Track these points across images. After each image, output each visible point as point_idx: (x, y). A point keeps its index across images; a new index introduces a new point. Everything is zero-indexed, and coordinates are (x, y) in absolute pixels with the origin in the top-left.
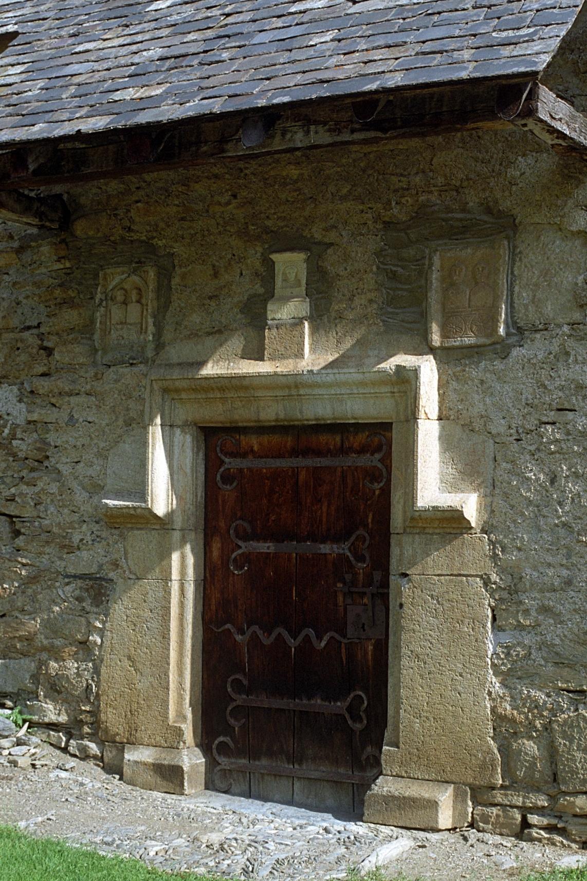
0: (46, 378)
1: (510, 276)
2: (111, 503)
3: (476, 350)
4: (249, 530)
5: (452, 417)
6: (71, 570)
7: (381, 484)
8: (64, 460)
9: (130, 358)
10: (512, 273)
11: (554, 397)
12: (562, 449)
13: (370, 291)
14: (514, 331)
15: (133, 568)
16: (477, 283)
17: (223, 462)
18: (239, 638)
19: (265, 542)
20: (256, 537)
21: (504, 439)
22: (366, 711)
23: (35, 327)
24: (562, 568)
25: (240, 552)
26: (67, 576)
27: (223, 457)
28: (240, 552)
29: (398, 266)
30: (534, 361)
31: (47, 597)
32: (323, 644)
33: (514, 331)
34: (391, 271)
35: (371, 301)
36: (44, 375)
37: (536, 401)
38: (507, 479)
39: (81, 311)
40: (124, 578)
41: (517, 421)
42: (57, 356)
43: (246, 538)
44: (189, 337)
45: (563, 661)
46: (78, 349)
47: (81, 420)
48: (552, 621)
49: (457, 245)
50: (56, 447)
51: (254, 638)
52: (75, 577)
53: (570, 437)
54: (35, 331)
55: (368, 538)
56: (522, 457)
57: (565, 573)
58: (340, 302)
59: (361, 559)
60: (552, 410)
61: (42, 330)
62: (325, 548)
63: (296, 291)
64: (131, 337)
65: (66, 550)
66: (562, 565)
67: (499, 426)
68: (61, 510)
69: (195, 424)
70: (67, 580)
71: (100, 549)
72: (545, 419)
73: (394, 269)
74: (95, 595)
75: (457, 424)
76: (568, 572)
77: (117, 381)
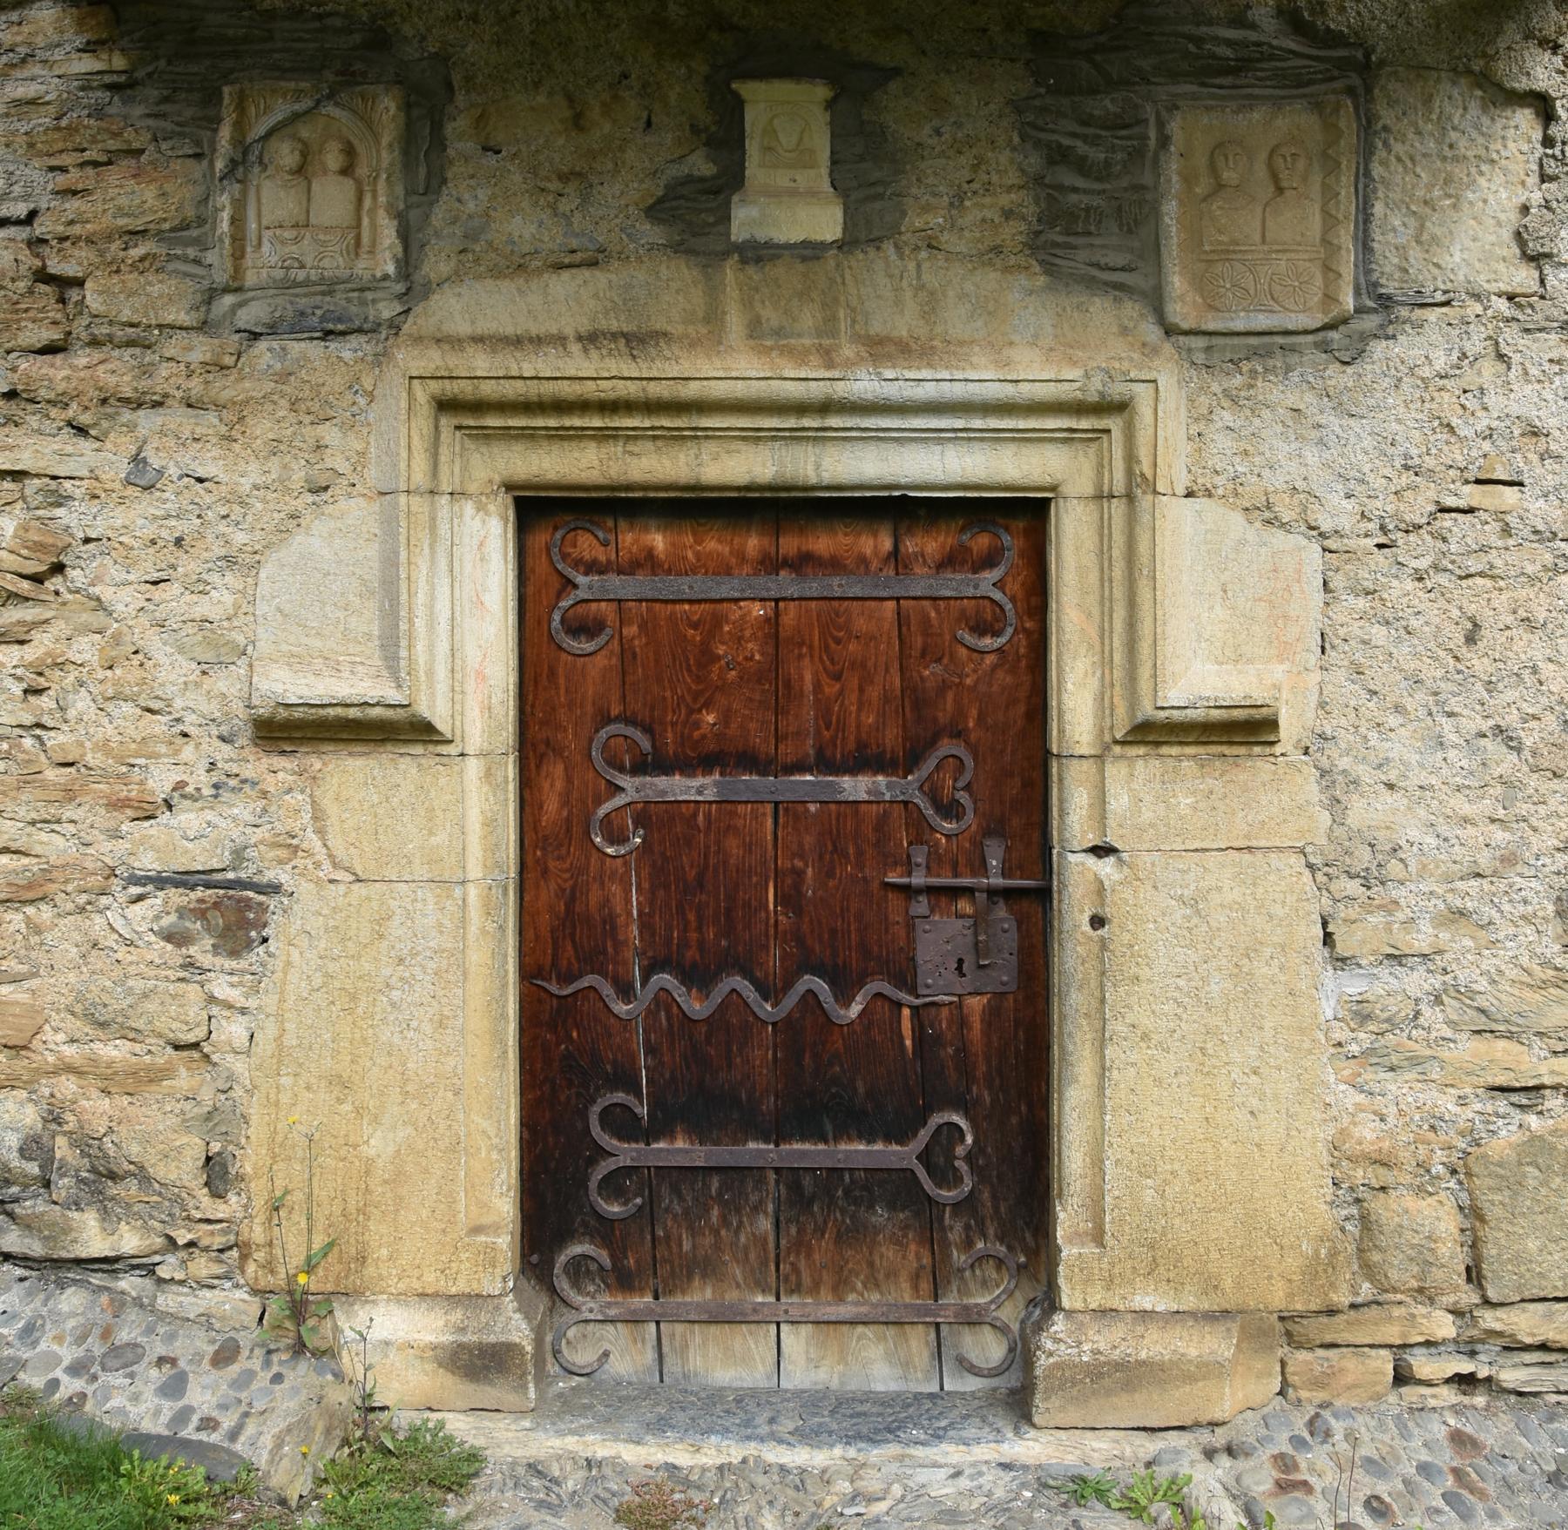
0: (58, 359)
1: (1362, 179)
2: (809, 778)
3: (1280, 340)
4: (646, 744)
5: (1220, 492)
6: (148, 863)
7: (1001, 640)
8: (117, 573)
9: (323, 319)
10: (1367, 174)
11: (1474, 453)
12: (1492, 567)
13: (1010, 189)
14: (1370, 304)
15: (340, 853)
16: (1280, 190)
17: (570, 584)
18: (621, 1008)
19: (692, 775)
20: (661, 765)
21: (1351, 543)
22: (969, 1158)
23: (19, 222)
24: (1493, 827)
25: (619, 800)
26: (134, 880)
27: (570, 572)
28: (619, 800)
29: (1074, 135)
30: (1426, 372)
31: (77, 937)
32: (855, 1009)
33: (1370, 304)
34: (1060, 145)
35: (1008, 214)
36: (50, 349)
37: (1430, 462)
38: (1359, 632)
39: (168, 187)
40: (318, 882)
41: (1383, 505)
42: (93, 299)
43: (640, 767)
44: (496, 273)
45: (1495, 1027)
46: (158, 287)
47: (173, 471)
48: (1468, 943)
49: (1223, 98)
50: (87, 541)
51: (663, 1000)
52: (160, 882)
53: (1511, 542)
54: (22, 233)
55: (969, 762)
56: (1395, 583)
57: (1499, 836)
58: (927, 209)
59: (951, 810)
60: (1467, 482)
61: (40, 228)
62: (855, 787)
63: (803, 179)
64: (326, 263)
65: (130, 813)
66: (1493, 821)
67: (1337, 512)
68: (110, 707)
69: (509, 487)
70: (135, 890)
71: (242, 809)
72: (1450, 501)
73: (1066, 142)
74: (227, 928)
75: (1233, 507)
76: (1507, 835)
77: (284, 377)
